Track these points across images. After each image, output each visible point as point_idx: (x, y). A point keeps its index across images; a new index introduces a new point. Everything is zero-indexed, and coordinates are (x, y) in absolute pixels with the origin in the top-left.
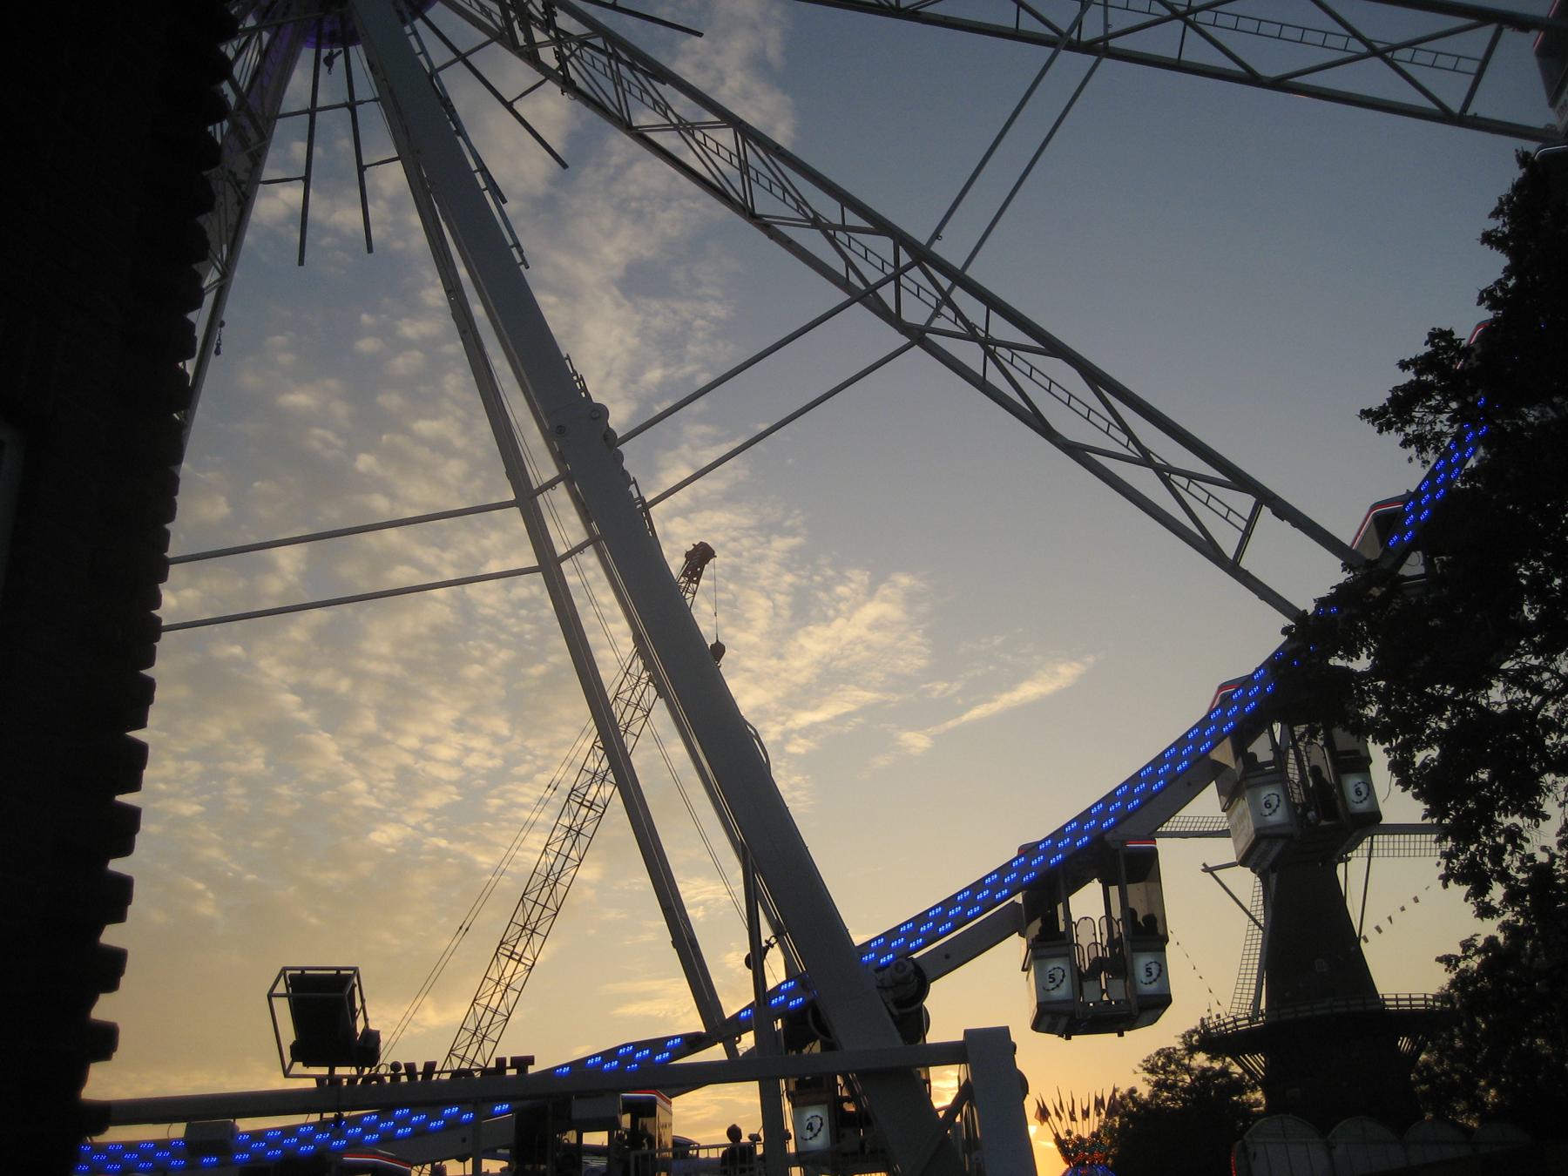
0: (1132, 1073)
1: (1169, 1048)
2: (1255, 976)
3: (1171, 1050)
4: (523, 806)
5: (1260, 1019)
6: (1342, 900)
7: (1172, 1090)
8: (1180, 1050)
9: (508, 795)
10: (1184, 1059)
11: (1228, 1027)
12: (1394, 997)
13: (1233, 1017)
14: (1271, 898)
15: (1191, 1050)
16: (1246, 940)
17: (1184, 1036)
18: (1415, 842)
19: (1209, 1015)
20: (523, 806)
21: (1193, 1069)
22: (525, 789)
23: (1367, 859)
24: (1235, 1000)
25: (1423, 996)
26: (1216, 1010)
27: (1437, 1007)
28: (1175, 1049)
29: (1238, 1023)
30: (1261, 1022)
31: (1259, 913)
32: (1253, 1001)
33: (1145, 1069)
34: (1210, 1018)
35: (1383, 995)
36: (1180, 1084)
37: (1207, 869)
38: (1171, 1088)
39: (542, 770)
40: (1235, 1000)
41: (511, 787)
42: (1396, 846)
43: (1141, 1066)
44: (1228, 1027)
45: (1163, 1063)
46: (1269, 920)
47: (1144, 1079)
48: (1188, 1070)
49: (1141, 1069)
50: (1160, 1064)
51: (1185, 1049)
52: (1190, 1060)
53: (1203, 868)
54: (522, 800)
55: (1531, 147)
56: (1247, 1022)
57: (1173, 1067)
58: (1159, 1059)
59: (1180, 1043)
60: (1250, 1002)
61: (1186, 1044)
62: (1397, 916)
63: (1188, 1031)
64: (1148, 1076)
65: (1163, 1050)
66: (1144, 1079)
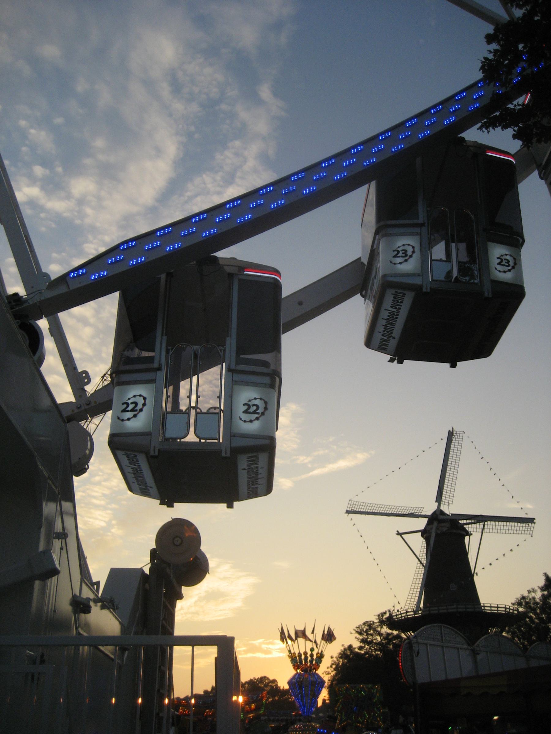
0: (349, 633)
1: (370, 621)
2: (419, 590)
3: (372, 623)
4: (95, 497)
5: (420, 612)
6: (466, 554)
7: (370, 644)
8: (376, 623)
9: (88, 491)
10: (378, 627)
11: (403, 615)
12: (496, 606)
13: (406, 610)
14: (430, 550)
15: (382, 623)
16: (414, 578)
17: (379, 616)
18: (509, 526)
19: (393, 609)
20: (95, 497)
21: (382, 634)
22: (96, 488)
23: (481, 533)
24: (407, 604)
25: (504, 606)
26: (398, 607)
27: (511, 612)
28: (373, 622)
29: (408, 614)
30: (420, 614)
31: (423, 557)
32: (417, 603)
33: (356, 632)
34: (394, 610)
35: (484, 604)
36: (375, 641)
37: (399, 534)
38: (370, 643)
39: (106, 480)
40: (407, 604)
41: (88, 487)
42: (499, 528)
43: (354, 630)
44: (403, 615)
45: (367, 630)
46: (428, 561)
47: (356, 638)
48: (380, 634)
49: (354, 632)
50: (365, 630)
51: (379, 622)
52: (381, 629)
53: (397, 533)
54: (95, 494)
55: (375, 694)
56: (412, 613)
57: (372, 632)
58: (364, 627)
59: (376, 619)
60: (415, 603)
61: (379, 620)
62: (508, 553)
63: (381, 613)
64: (358, 636)
65: (367, 622)
66: (356, 638)
